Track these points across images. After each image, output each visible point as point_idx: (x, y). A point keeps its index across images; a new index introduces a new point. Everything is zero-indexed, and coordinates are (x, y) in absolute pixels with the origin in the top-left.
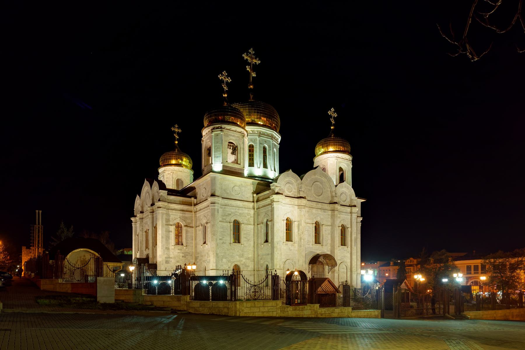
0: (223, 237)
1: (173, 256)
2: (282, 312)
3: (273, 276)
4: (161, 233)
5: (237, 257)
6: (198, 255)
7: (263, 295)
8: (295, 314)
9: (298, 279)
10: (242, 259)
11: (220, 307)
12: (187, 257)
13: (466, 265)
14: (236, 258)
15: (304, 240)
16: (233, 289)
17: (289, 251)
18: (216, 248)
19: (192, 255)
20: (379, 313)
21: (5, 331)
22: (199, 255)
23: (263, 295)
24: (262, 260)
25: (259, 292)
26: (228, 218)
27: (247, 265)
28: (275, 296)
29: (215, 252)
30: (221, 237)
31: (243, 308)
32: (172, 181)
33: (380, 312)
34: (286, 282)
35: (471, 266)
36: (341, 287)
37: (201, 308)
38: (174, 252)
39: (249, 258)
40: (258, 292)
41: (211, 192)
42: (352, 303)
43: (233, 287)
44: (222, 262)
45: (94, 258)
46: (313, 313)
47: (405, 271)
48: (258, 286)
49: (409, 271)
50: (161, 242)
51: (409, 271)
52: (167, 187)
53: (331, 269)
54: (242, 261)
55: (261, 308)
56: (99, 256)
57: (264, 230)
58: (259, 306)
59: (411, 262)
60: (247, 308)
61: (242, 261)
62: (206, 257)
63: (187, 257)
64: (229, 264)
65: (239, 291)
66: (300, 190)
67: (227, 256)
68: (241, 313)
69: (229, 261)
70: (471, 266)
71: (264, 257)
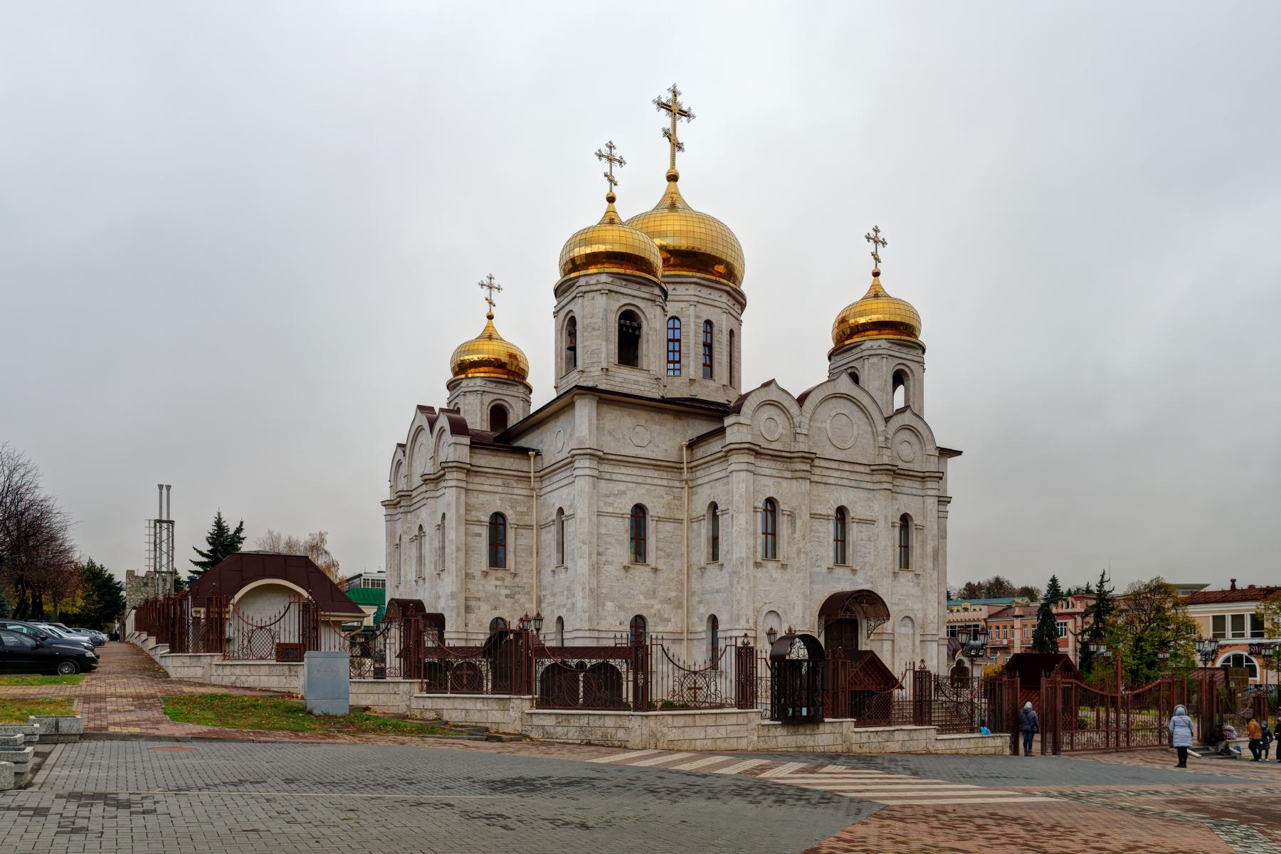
0: (607, 549)
1: (484, 595)
2: (762, 738)
3: (739, 648)
4: (454, 538)
5: (641, 597)
6: (543, 593)
7: (713, 696)
8: (794, 745)
9: (801, 657)
10: (652, 602)
12: (517, 596)
13: (1211, 615)
14: (639, 600)
15: (806, 553)
16: (641, 682)
17: (769, 583)
18: (589, 575)
19: (528, 593)
20: (1006, 742)
21: (88, 809)
22: (547, 592)
23: (713, 696)
24: (701, 605)
26: (619, 501)
27: (666, 616)
28: (745, 697)
29: (587, 586)
31: (665, 730)
32: (481, 411)
33: (1008, 739)
34: (772, 664)
35: (1224, 617)
36: (910, 675)
37: (559, 729)
38: (487, 586)
39: (670, 599)
40: (701, 688)
42: (938, 715)
43: (641, 676)
44: (603, 610)
45: (299, 602)
46: (840, 741)
47: (1056, 630)
49: (1062, 631)
50: (454, 561)
51: (1062, 631)
52: (470, 426)
54: (652, 606)
55: (710, 730)
56: (310, 598)
57: (708, 529)
58: (704, 724)
59: (1068, 607)
60: (674, 730)
61: (652, 606)
62: (565, 598)
64: (622, 614)
65: (654, 688)
66: (799, 431)
67: (617, 596)
68: (661, 742)
69: (621, 607)
70: (1224, 617)
71: (708, 596)
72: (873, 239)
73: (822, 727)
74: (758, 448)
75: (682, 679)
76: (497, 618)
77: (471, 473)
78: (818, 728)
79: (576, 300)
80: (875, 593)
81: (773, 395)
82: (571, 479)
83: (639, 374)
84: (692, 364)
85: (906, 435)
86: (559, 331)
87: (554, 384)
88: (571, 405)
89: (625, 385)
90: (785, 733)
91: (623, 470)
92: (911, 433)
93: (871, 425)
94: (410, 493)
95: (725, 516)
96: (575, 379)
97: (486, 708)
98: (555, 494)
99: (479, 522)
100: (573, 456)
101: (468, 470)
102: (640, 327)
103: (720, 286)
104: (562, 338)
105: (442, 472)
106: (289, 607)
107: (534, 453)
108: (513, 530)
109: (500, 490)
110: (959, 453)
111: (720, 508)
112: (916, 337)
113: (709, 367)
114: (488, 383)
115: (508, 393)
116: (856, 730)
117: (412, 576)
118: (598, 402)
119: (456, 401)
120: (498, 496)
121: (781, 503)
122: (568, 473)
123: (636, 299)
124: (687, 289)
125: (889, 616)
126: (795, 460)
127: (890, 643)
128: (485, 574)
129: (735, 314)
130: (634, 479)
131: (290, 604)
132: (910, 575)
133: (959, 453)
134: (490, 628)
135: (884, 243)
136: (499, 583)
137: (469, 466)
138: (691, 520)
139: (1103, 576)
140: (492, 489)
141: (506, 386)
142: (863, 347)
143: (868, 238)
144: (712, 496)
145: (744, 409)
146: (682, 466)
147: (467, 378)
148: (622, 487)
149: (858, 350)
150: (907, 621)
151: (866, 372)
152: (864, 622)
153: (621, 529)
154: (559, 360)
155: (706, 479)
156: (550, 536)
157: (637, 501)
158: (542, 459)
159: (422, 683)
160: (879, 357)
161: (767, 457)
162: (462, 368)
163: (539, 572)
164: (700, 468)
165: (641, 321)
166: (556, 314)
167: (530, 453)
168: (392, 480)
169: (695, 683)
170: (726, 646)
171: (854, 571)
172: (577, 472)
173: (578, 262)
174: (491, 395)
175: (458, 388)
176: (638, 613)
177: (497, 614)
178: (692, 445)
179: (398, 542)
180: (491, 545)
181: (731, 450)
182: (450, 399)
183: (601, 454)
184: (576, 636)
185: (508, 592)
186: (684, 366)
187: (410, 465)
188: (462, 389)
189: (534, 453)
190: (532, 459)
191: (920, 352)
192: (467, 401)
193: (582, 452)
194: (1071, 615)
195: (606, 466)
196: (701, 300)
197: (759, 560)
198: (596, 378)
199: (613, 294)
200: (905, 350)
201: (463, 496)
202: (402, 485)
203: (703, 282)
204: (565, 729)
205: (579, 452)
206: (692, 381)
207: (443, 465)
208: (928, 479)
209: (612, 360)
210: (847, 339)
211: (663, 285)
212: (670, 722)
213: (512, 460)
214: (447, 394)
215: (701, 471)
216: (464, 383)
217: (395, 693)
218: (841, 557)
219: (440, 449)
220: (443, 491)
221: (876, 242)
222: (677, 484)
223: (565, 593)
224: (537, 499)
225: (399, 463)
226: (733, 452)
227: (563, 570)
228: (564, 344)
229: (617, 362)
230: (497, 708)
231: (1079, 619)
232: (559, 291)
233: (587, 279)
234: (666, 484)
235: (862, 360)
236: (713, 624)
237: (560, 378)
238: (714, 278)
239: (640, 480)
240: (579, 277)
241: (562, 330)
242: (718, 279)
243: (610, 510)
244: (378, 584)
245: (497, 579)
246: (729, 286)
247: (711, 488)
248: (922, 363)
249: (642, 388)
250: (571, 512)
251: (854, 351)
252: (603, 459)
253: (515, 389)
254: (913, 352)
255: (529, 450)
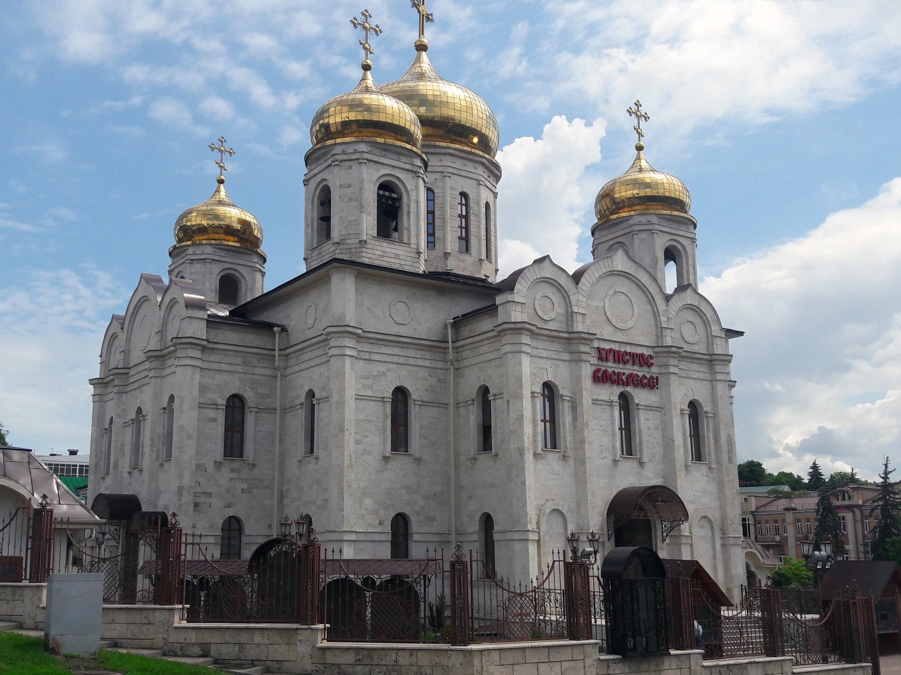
11: (402, 664)
12: (255, 491)
25: (533, 617)
30: (359, 437)
37: (359, 668)
40: (529, 615)
41: (497, 318)
48: (528, 594)
53: (672, 529)
57: (477, 416)
59: (844, 499)
63: (255, 491)
72: (636, 113)
73: (667, 661)
74: (534, 328)
75: (507, 603)
76: (230, 517)
77: (206, 350)
78: (663, 663)
79: (330, 168)
80: (670, 490)
81: (546, 271)
82: (324, 359)
83: (399, 247)
84: (451, 240)
85: (690, 316)
86: (309, 200)
87: (303, 256)
88: (326, 279)
89: (385, 259)
90: (627, 670)
91: (384, 350)
92: (694, 312)
93: (651, 304)
94: (127, 371)
95: (498, 401)
96: (328, 252)
97: (266, 642)
98: (304, 374)
99: (215, 405)
100: (329, 334)
101: (204, 347)
102: (400, 199)
103: (438, 150)
104: (313, 207)
105: (172, 348)
106: (16, 513)
107: (280, 329)
108: (253, 414)
109: (239, 369)
110: (741, 334)
111: (492, 392)
112: (686, 212)
113: (465, 240)
114: (218, 251)
115: (241, 262)
116: (706, 663)
117: (125, 465)
118: (356, 277)
119: (180, 268)
120: (236, 376)
121: (560, 389)
122: (320, 352)
123: (395, 169)
124: (441, 160)
125: (688, 517)
126: (574, 341)
127: (689, 547)
128: (218, 465)
129: (490, 186)
130: (395, 359)
131: (18, 509)
132: (704, 469)
133: (741, 334)
134: (222, 530)
135: (646, 118)
136: (234, 475)
137: (205, 343)
138: (457, 405)
139: (886, 465)
140: (231, 368)
141: (238, 255)
142: (631, 222)
143: (630, 112)
144: (482, 378)
145: (518, 286)
146: (447, 345)
147: (194, 244)
148: (382, 368)
149: (626, 225)
150: (704, 522)
151: (636, 248)
152: (658, 522)
153: (382, 415)
154: (310, 230)
155: (476, 360)
156: (297, 422)
157: (397, 384)
158: (288, 335)
159: (183, 609)
160: (650, 232)
161: (543, 338)
162: (186, 233)
163: (282, 463)
164: (466, 348)
165: (402, 193)
166: (306, 182)
167: (275, 329)
168: (104, 355)
169: (521, 608)
170: (554, 562)
171: (641, 464)
172: (333, 352)
173: (333, 129)
174: (222, 264)
175: (183, 255)
176: (400, 511)
177: (230, 512)
178: (458, 323)
179: (107, 426)
180: (226, 430)
181: (505, 330)
182: (172, 267)
183: (360, 332)
184: (329, 538)
185: (245, 486)
186: (439, 239)
187: (129, 339)
188: (188, 257)
189: (280, 329)
190: (277, 335)
191: (692, 228)
192: (193, 270)
193: (340, 329)
194: (850, 508)
195: (347, 339)
196: (455, 171)
197: (539, 451)
198: (354, 250)
199: (372, 164)
200: (675, 226)
201: (197, 376)
202: (117, 360)
203: (457, 153)
204: (367, 669)
205: (335, 329)
206: (446, 255)
207: (174, 340)
208: (717, 363)
209: (370, 232)
210: (612, 214)
211: (424, 156)
212: (497, 658)
213: (253, 336)
214: (169, 261)
215: (469, 352)
216: (190, 251)
217: (149, 623)
218: (629, 447)
219: (170, 323)
220: (173, 369)
221: (638, 117)
222: (440, 365)
223: (315, 487)
224: (281, 379)
225: (114, 337)
226: (508, 332)
227: (313, 461)
228: (315, 214)
229: (375, 235)
230: (281, 642)
231: (858, 512)
232: (309, 159)
233: (344, 147)
234: (430, 365)
235: (630, 235)
236: (486, 523)
237: (311, 249)
238: (469, 149)
239: (401, 360)
240: (335, 144)
241: (313, 198)
242: (473, 150)
243: (370, 393)
244: (68, 471)
245: (232, 470)
246: (485, 158)
247: (481, 370)
248: (693, 240)
249: (403, 263)
250: (324, 394)
251: (621, 226)
252: (362, 337)
253: (247, 258)
254: (683, 227)
255: (274, 325)
